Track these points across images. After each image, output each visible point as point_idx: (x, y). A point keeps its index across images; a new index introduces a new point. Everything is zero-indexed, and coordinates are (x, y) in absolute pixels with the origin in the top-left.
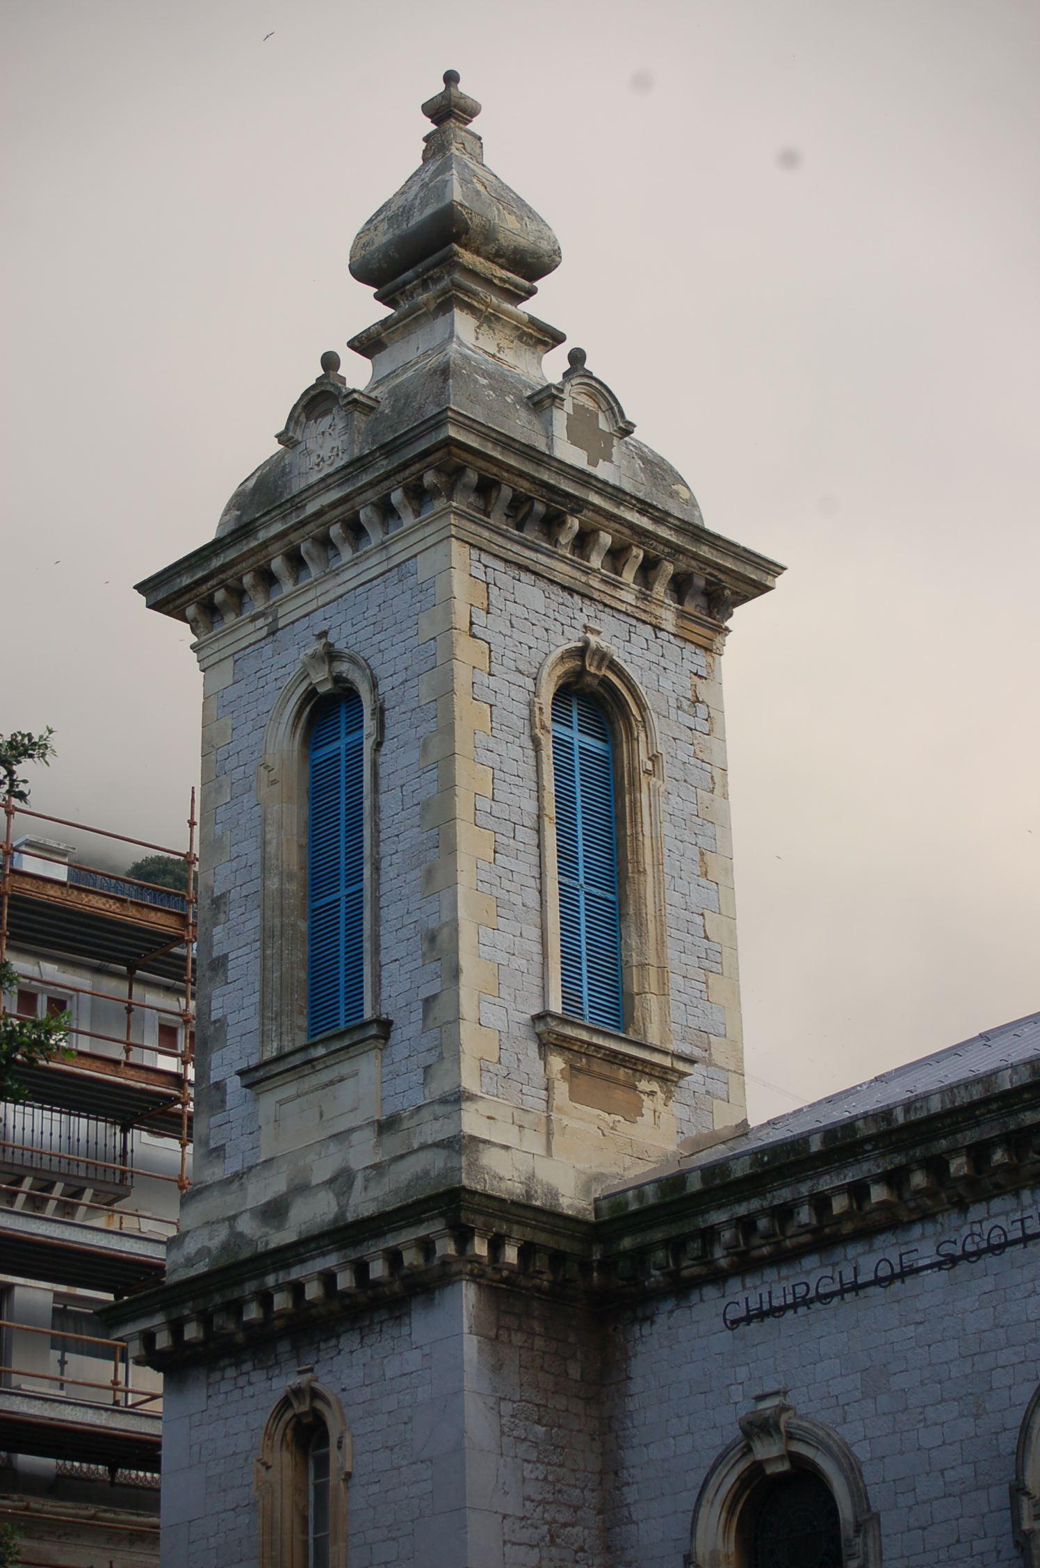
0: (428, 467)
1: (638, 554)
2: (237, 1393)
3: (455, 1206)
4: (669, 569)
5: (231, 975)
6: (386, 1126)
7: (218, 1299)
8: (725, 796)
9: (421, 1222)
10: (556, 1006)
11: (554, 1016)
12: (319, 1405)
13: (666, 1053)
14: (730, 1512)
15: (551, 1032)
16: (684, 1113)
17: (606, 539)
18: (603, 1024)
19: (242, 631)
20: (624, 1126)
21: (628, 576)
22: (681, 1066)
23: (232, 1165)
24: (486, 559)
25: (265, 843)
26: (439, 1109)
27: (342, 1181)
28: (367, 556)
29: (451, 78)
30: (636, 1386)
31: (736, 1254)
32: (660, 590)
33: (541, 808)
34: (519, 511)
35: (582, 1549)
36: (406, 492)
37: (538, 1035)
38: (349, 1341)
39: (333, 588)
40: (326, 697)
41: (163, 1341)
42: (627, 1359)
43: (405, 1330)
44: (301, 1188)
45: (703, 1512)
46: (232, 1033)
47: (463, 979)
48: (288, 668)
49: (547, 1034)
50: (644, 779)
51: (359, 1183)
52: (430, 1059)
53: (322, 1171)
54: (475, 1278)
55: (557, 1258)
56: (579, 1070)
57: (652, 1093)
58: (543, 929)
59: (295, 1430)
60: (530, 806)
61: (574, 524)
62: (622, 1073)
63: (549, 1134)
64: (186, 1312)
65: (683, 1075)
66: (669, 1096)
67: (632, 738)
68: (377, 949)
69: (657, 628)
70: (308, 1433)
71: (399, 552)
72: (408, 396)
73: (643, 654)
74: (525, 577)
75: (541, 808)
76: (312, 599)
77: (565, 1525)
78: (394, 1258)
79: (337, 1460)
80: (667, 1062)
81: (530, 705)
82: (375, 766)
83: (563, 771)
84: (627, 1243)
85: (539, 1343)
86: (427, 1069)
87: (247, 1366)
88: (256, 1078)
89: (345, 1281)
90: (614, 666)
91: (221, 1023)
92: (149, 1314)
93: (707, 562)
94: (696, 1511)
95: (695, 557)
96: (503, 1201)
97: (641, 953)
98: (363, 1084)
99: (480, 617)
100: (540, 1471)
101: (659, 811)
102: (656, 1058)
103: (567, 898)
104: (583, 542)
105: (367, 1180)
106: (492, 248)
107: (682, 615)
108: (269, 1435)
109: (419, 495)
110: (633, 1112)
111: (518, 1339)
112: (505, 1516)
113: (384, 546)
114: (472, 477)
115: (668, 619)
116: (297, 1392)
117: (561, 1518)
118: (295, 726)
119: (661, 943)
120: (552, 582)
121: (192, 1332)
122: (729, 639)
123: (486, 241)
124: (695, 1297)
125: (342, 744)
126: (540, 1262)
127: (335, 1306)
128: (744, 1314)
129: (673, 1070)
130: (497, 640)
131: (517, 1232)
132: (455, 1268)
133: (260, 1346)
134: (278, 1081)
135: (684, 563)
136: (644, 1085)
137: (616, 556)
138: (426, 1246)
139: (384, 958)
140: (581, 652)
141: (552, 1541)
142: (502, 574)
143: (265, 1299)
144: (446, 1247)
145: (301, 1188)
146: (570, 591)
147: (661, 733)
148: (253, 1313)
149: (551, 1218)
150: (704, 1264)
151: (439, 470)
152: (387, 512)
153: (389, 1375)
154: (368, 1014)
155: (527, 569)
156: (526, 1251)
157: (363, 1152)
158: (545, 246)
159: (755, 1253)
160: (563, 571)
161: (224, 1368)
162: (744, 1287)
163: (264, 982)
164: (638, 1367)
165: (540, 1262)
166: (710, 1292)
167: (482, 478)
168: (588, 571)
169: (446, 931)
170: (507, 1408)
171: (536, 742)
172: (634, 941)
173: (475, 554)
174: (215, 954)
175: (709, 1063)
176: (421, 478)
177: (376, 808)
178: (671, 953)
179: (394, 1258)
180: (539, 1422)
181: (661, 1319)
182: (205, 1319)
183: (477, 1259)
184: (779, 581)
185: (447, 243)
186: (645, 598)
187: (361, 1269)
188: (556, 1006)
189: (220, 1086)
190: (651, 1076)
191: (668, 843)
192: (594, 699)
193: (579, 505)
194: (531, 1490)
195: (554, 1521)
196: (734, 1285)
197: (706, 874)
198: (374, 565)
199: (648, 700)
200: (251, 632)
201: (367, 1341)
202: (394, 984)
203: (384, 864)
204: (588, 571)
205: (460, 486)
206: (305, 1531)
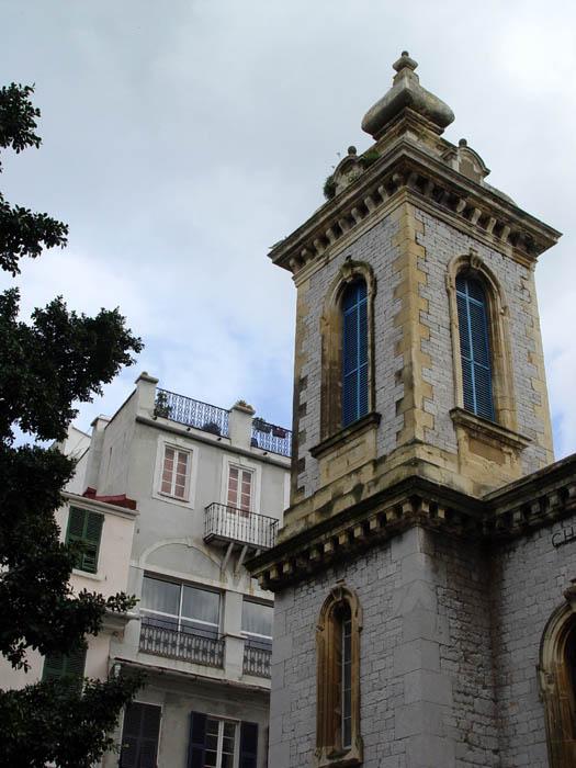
0: (394, 173)
1: (493, 221)
2: (308, 597)
3: (415, 488)
4: (508, 230)
5: (308, 411)
6: (376, 463)
7: (298, 551)
8: (539, 330)
9: (394, 498)
10: (461, 405)
11: (461, 410)
12: (347, 597)
13: (516, 434)
14: (560, 642)
15: (459, 417)
16: (525, 465)
17: (479, 212)
18: (483, 421)
19: (313, 266)
20: (496, 467)
21: (490, 230)
22: (523, 442)
23: (308, 494)
24: (422, 213)
25: (323, 350)
26: (404, 449)
27: (358, 489)
28: (368, 219)
29: (405, 65)
30: (507, 584)
31: (559, 509)
32: (504, 238)
33: (451, 320)
34: (437, 194)
35: (481, 666)
36: (385, 187)
37: (453, 419)
38: (361, 564)
39: (353, 237)
40: (349, 285)
41: (273, 575)
42: (502, 571)
43: (388, 555)
44: (338, 496)
45: (546, 642)
46: (308, 436)
47: (416, 389)
48: (329, 276)
49: (458, 418)
50: (500, 316)
51: (366, 488)
52: (400, 428)
53: (348, 486)
54: (423, 525)
55: (465, 519)
56: (473, 438)
57: (510, 454)
58: (454, 373)
59: (335, 610)
60: (447, 319)
61: (463, 203)
62: (494, 443)
63: (460, 464)
64: (284, 559)
65: (525, 446)
66: (518, 456)
67: (493, 299)
68: (374, 384)
69: (503, 255)
70: (341, 612)
71: (383, 213)
72: (419, 601)
73: (500, 264)
74: (441, 223)
75: (451, 320)
76: (342, 246)
77: (472, 653)
78: (382, 518)
79: (355, 622)
80: (516, 439)
81: (445, 276)
82: (372, 305)
83: (461, 310)
84: (501, 511)
85: (456, 561)
86: (398, 433)
87: (313, 584)
88: (317, 452)
89: (358, 532)
90: (483, 266)
91: (304, 432)
92: (267, 562)
93: (526, 227)
94: (542, 647)
95: (521, 224)
96: (436, 485)
97: (501, 392)
98: (369, 445)
99: (420, 236)
100: (458, 624)
101: (508, 331)
102: (511, 436)
103: (465, 365)
104: (468, 213)
105: (369, 487)
106: (424, 111)
107: (515, 251)
108: (322, 614)
109: (391, 188)
110: (501, 462)
111: (445, 557)
112: (440, 645)
113: (376, 213)
114: (415, 175)
115: (509, 251)
116: (335, 592)
117: (471, 648)
118: (337, 299)
119: (511, 388)
120: (454, 228)
121: (286, 568)
122: (537, 265)
123: (420, 107)
124: (537, 536)
125: (358, 305)
126: (456, 519)
127: (354, 547)
128: (563, 539)
129: (520, 443)
130: (429, 248)
131: (443, 503)
132: (413, 520)
133: (317, 573)
134: (328, 451)
135: (516, 227)
136: (505, 449)
137: (483, 221)
138: (398, 509)
139: (377, 388)
140: (467, 258)
141: (466, 661)
142: (432, 222)
143: (320, 547)
144: (407, 508)
145: (338, 496)
146: (463, 233)
147: (507, 297)
148: (314, 555)
149: (459, 496)
150: (542, 517)
151: (400, 173)
152: (377, 199)
153: (380, 577)
154: (370, 411)
155: (442, 220)
156: (449, 512)
157: (368, 475)
158: (448, 113)
159: (568, 508)
160: (460, 224)
161: (302, 587)
162: (562, 527)
163: (322, 410)
164: (508, 574)
165: (456, 519)
166: (545, 532)
167: (420, 177)
168: (471, 225)
169: (406, 369)
170: (440, 591)
171: (448, 291)
172: (498, 387)
173: (417, 210)
174: (301, 403)
175: (537, 444)
176: (391, 179)
177: (373, 324)
178: (516, 393)
179: (382, 518)
180: (457, 599)
181: (519, 549)
182: (292, 563)
183: (423, 515)
184: (559, 240)
185: (403, 107)
186: (498, 241)
187: (366, 526)
188: (461, 405)
189: (303, 460)
190: (509, 446)
191: (513, 346)
192: (474, 281)
193: (465, 194)
194: (454, 633)
195: (467, 650)
196: (557, 527)
197: (531, 361)
198: (371, 222)
199: (500, 282)
200: (317, 265)
201: (370, 563)
202: (386, 395)
203: (377, 347)
204: (471, 225)
205: (409, 180)
206: (340, 661)
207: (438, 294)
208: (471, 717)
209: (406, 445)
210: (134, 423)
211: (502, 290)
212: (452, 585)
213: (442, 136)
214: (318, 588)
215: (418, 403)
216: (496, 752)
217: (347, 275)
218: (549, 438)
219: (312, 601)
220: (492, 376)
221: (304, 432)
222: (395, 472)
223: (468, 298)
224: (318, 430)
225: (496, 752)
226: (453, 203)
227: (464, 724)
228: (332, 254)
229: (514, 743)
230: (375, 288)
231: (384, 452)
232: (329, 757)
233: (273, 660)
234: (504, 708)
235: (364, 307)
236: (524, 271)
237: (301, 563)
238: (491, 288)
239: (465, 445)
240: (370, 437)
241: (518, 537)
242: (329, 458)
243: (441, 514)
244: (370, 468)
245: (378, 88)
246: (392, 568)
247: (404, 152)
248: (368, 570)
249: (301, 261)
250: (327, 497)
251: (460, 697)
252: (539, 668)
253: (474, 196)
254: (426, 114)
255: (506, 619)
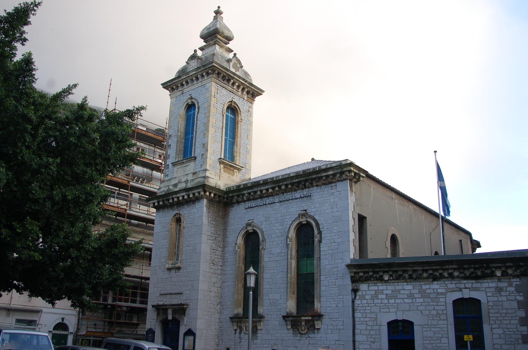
1: (242, 87)
3: (204, 187)
6: (194, 174)
10: (223, 157)
16: (241, 175)
17: (237, 84)
18: (229, 161)
19: (177, 93)
20: (232, 177)
21: (240, 90)
27: (187, 181)
32: (245, 93)
34: (224, 78)
38: (186, 206)
39: (193, 87)
40: (190, 105)
41: (156, 204)
44: (180, 182)
48: (184, 100)
54: (206, 198)
55: (219, 196)
60: (221, 125)
61: (232, 81)
67: (238, 116)
68: (195, 146)
70: (178, 220)
73: (241, 102)
83: (227, 120)
84: (230, 195)
88: (174, 164)
89: (186, 197)
90: (236, 104)
91: (169, 155)
92: (154, 200)
98: (191, 167)
99: (216, 94)
101: (241, 128)
103: (226, 140)
104: (233, 84)
107: (248, 97)
108: (172, 220)
109: (208, 74)
110: (233, 175)
111: (212, 208)
113: (201, 81)
114: (217, 72)
115: (246, 98)
119: (240, 149)
123: (222, 34)
126: (217, 197)
131: (213, 192)
133: (171, 206)
136: (235, 171)
137: (238, 87)
138: (199, 193)
144: (202, 193)
145: (180, 182)
147: (243, 115)
148: (171, 201)
151: (211, 70)
152: (203, 76)
156: (215, 195)
158: (231, 36)
160: (230, 88)
164: (230, 214)
165: (217, 197)
166: (243, 203)
168: (234, 89)
170: (210, 219)
171: (223, 115)
175: (246, 168)
177: (197, 123)
179: (194, 194)
181: (235, 207)
182: (163, 201)
187: (188, 195)
188: (223, 157)
189: (168, 165)
192: (233, 109)
193: (233, 78)
196: (247, 203)
200: (179, 93)
202: (197, 151)
204: (234, 89)
207: (220, 116)
208: (215, 256)
209: (203, 170)
210: (167, 271)
211: (242, 113)
212: (214, 217)
213: (228, 46)
214: (171, 211)
215: (209, 156)
216: (221, 266)
217: (189, 101)
218: (250, 166)
219: (169, 215)
220: (234, 144)
221: (169, 155)
222: (198, 181)
223: (230, 115)
224: (175, 156)
225: (221, 266)
226: (229, 81)
227: (212, 259)
228: (185, 91)
229: (226, 264)
230: (199, 110)
231: (197, 170)
232: (172, 264)
233: (155, 231)
234: (225, 254)
235: (194, 114)
236: (250, 104)
237: (166, 202)
238: (238, 112)
239: (222, 170)
240: (192, 164)
241: (235, 203)
242: (178, 167)
243: (212, 195)
244: (191, 175)
245: (206, 20)
246: (196, 210)
247: (214, 64)
248: (188, 209)
249: (173, 89)
250: (176, 181)
251: (212, 251)
252: (236, 244)
253: (236, 79)
254: (223, 37)
255: (228, 228)
